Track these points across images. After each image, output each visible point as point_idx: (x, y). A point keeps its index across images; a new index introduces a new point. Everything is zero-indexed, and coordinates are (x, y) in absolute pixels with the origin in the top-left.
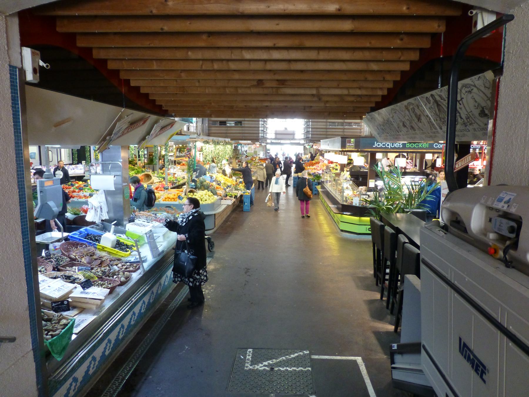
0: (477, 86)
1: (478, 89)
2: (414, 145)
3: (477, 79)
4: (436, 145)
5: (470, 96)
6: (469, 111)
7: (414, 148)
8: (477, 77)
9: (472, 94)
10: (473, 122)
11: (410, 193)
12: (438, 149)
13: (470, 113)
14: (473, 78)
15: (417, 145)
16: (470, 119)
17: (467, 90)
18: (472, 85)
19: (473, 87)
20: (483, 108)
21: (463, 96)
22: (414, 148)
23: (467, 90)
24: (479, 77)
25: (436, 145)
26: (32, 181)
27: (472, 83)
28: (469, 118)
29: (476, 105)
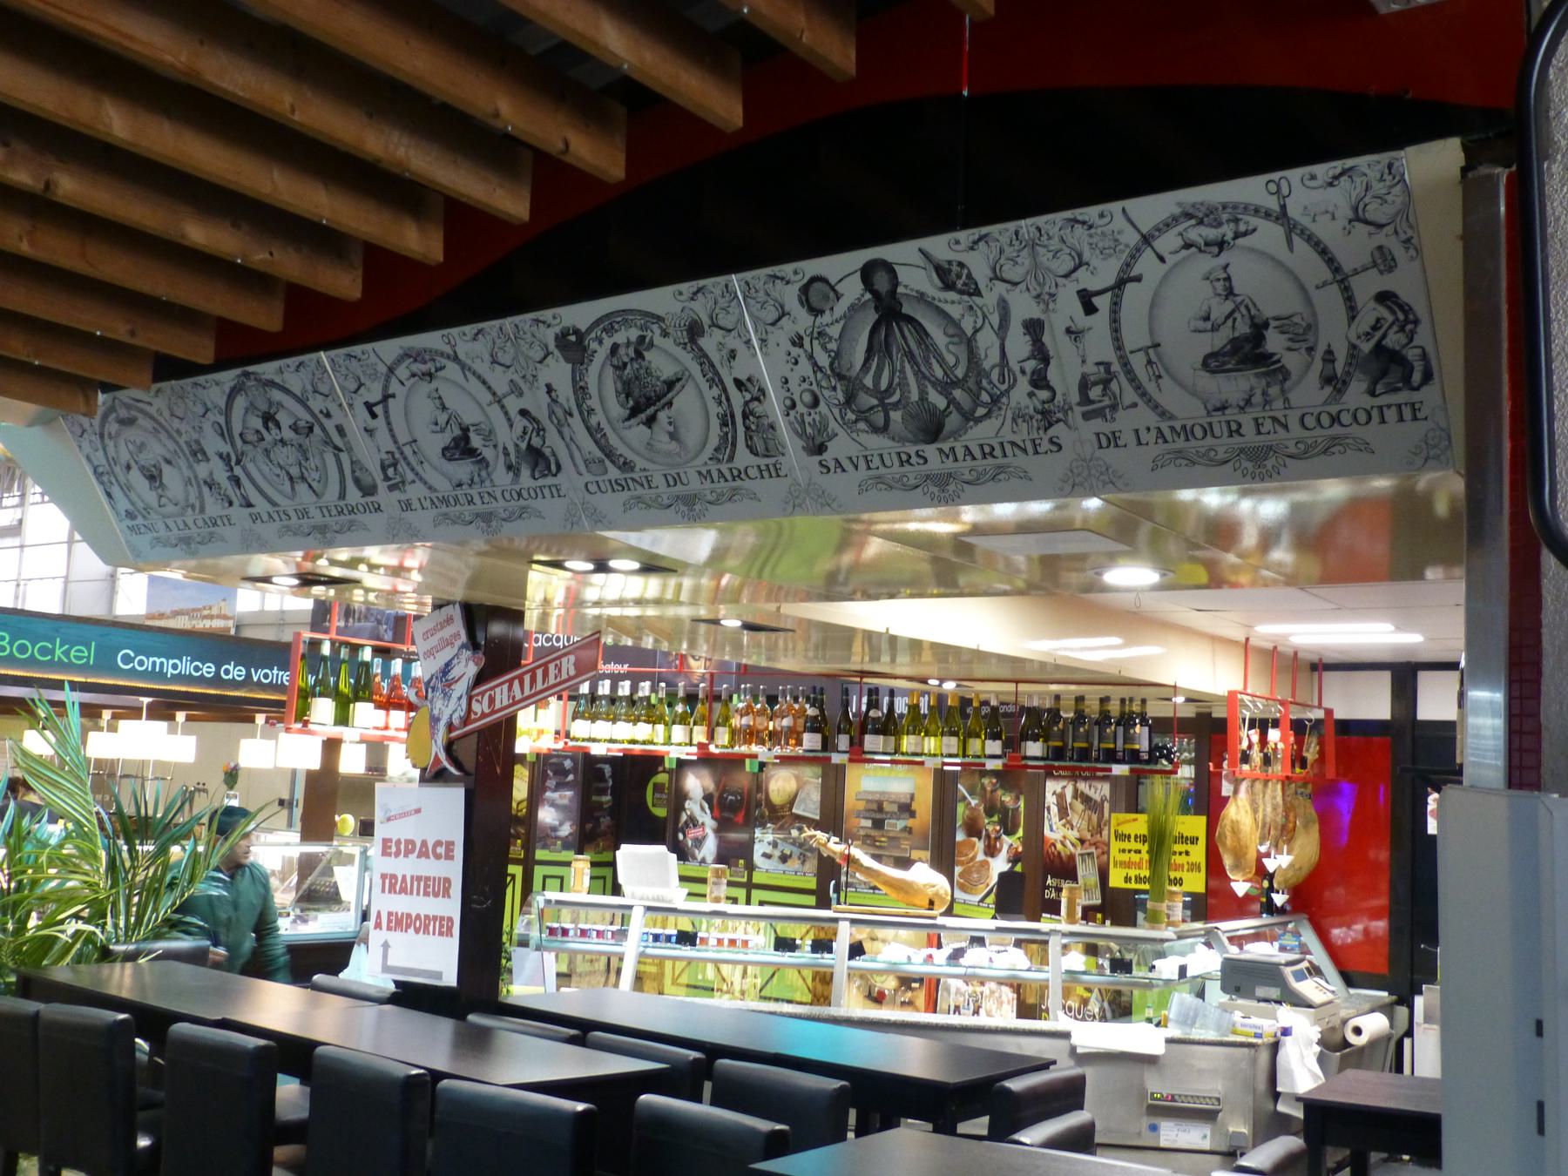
0: (461, 356)
1: (463, 367)
2: (34, 650)
3: (468, 338)
4: (127, 660)
5: (425, 387)
6: (403, 438)
7: (31, 662)
8: (470, 329)
9: (435, 384)
10: (410, 476)
11: (1106, 589)
12: (133, 673)
13: (407, 450)
14: (455, 331)
15: (43, 651)
16: (402, 467)
17: (419, 367)
18: (442, 354)
19: (444, 361)
20: (465, 430)
21: (394, 387)
22: (31, 662)
23: (419, 367)
24: (480, 332)
25: (127, 660)
26: (1022, 804)
27: (448, 349)
28: (395, 465)
29: (442, 419)
